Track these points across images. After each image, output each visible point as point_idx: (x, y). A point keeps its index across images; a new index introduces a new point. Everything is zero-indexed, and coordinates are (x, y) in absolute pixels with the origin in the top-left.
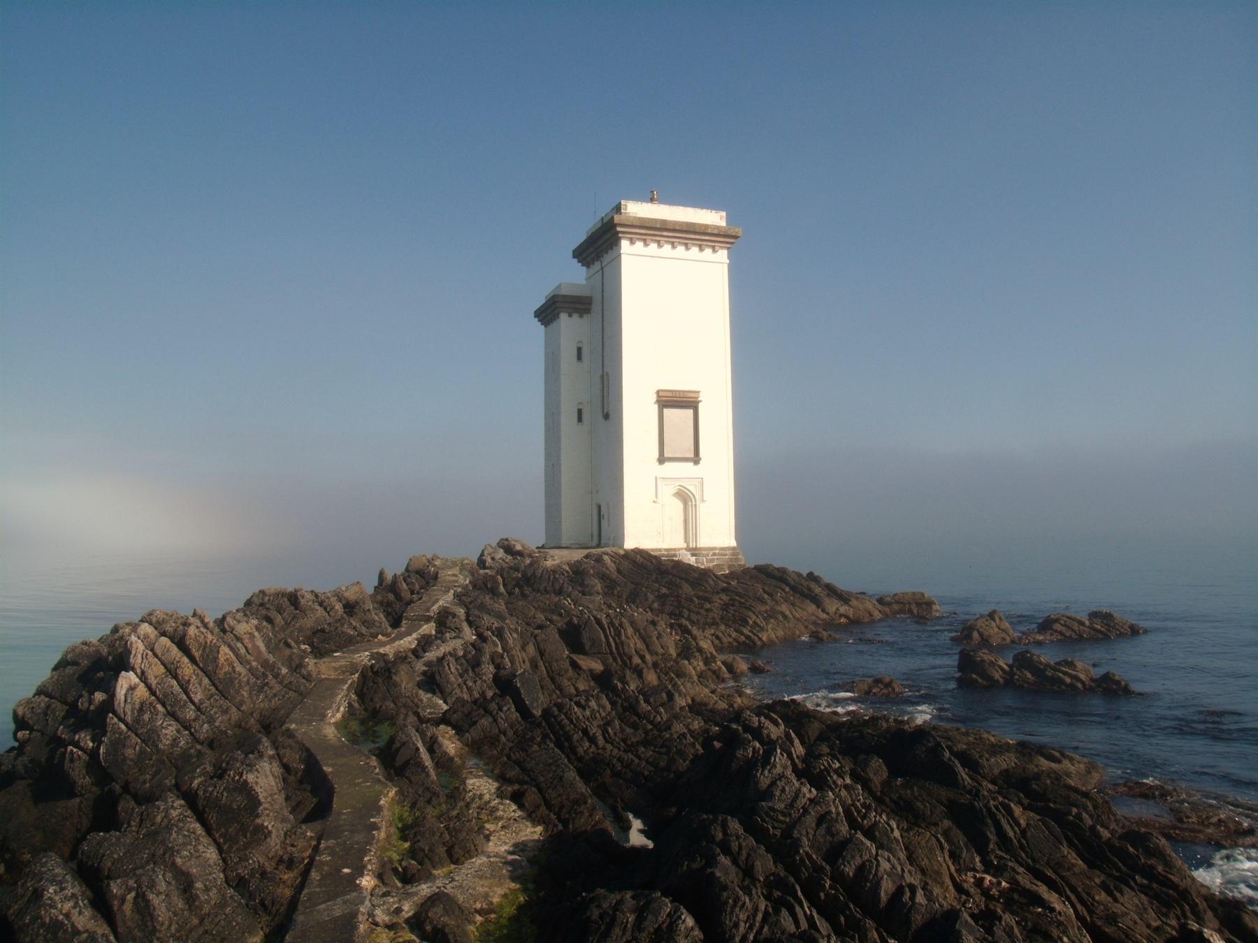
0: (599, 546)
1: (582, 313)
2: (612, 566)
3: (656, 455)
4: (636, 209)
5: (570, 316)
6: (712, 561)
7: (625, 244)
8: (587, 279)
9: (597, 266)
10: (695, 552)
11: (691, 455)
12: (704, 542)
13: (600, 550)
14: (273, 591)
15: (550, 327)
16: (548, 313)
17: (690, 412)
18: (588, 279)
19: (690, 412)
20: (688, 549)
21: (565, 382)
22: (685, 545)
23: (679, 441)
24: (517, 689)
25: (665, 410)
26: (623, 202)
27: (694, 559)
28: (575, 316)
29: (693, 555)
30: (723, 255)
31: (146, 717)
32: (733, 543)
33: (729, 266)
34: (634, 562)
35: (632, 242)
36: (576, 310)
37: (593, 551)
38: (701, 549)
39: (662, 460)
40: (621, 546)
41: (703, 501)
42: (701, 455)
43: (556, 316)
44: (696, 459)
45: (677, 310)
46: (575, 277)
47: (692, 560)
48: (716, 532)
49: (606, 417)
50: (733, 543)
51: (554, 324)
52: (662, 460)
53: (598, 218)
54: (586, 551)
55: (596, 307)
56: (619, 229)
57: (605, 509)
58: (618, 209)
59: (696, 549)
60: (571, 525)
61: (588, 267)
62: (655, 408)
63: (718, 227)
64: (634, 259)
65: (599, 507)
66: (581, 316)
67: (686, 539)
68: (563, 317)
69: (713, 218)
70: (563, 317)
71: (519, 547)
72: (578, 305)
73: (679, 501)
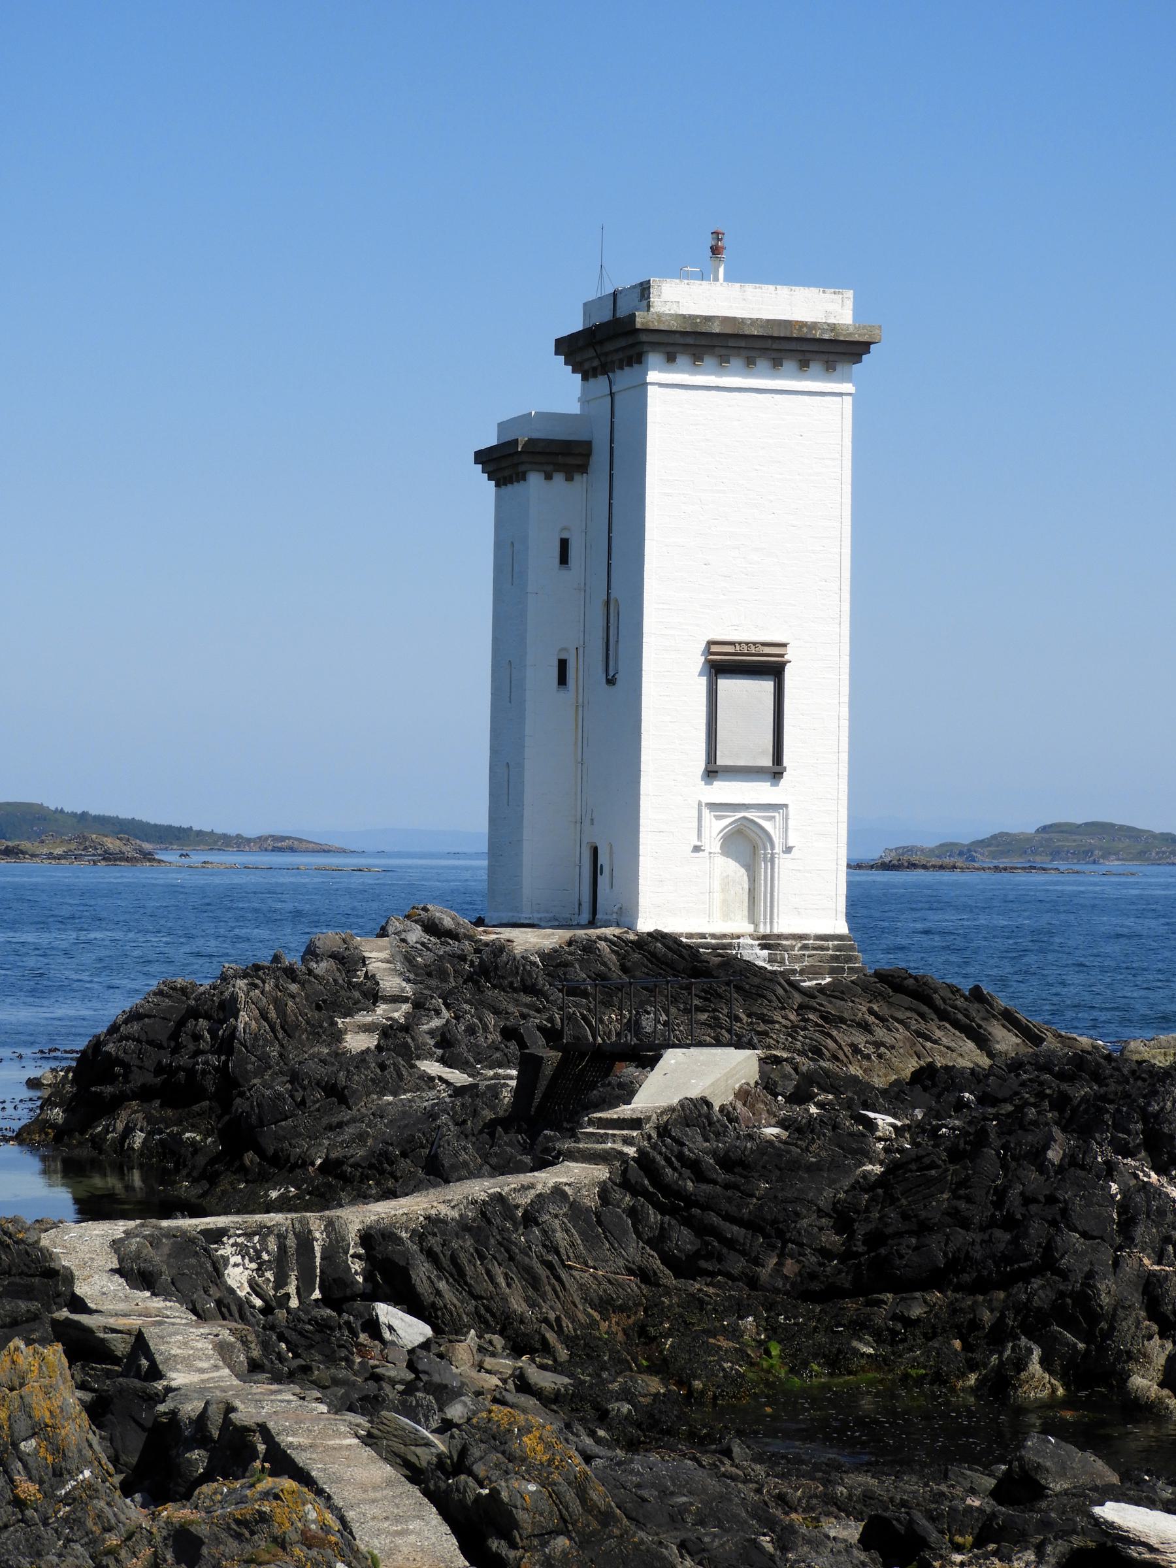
0: (592, 924)
3: (702, 765)
4: (680, 298)
5: (548, 477)
10: (769, 942)
11: (767, 761)
12: (785, 924)
13: (593, 932)
14: (34, 1155)
15: (509, 489)
16: (504, 462)
17: (768, 685)
18: (584, 400)
22: (750, 929)
23: (745, 741)
25: (724, 684)
28: (559, 478)
29: (764, 947)
32: (842, 928)
34: (653, 956)
36: (560, 468)
37: (581, 933)
38: (780, 936)
39: (712, 772)
40: (626, 913)
42: (787, 760)
44: (776, 772)
45: (743, 501)
46: (560, 393)
47: (759, 957)
49: (611, 681)
50: (842, 928)
52: (712, 772)
54: (567, 934)
56: (644, 338)
57: (601, 871)
58: (644, 290)
60: (544, 863)
61: (585, 378)
62: (701, 684)
64: (680, 411)
65: (595, 850)
66: (569, 478)
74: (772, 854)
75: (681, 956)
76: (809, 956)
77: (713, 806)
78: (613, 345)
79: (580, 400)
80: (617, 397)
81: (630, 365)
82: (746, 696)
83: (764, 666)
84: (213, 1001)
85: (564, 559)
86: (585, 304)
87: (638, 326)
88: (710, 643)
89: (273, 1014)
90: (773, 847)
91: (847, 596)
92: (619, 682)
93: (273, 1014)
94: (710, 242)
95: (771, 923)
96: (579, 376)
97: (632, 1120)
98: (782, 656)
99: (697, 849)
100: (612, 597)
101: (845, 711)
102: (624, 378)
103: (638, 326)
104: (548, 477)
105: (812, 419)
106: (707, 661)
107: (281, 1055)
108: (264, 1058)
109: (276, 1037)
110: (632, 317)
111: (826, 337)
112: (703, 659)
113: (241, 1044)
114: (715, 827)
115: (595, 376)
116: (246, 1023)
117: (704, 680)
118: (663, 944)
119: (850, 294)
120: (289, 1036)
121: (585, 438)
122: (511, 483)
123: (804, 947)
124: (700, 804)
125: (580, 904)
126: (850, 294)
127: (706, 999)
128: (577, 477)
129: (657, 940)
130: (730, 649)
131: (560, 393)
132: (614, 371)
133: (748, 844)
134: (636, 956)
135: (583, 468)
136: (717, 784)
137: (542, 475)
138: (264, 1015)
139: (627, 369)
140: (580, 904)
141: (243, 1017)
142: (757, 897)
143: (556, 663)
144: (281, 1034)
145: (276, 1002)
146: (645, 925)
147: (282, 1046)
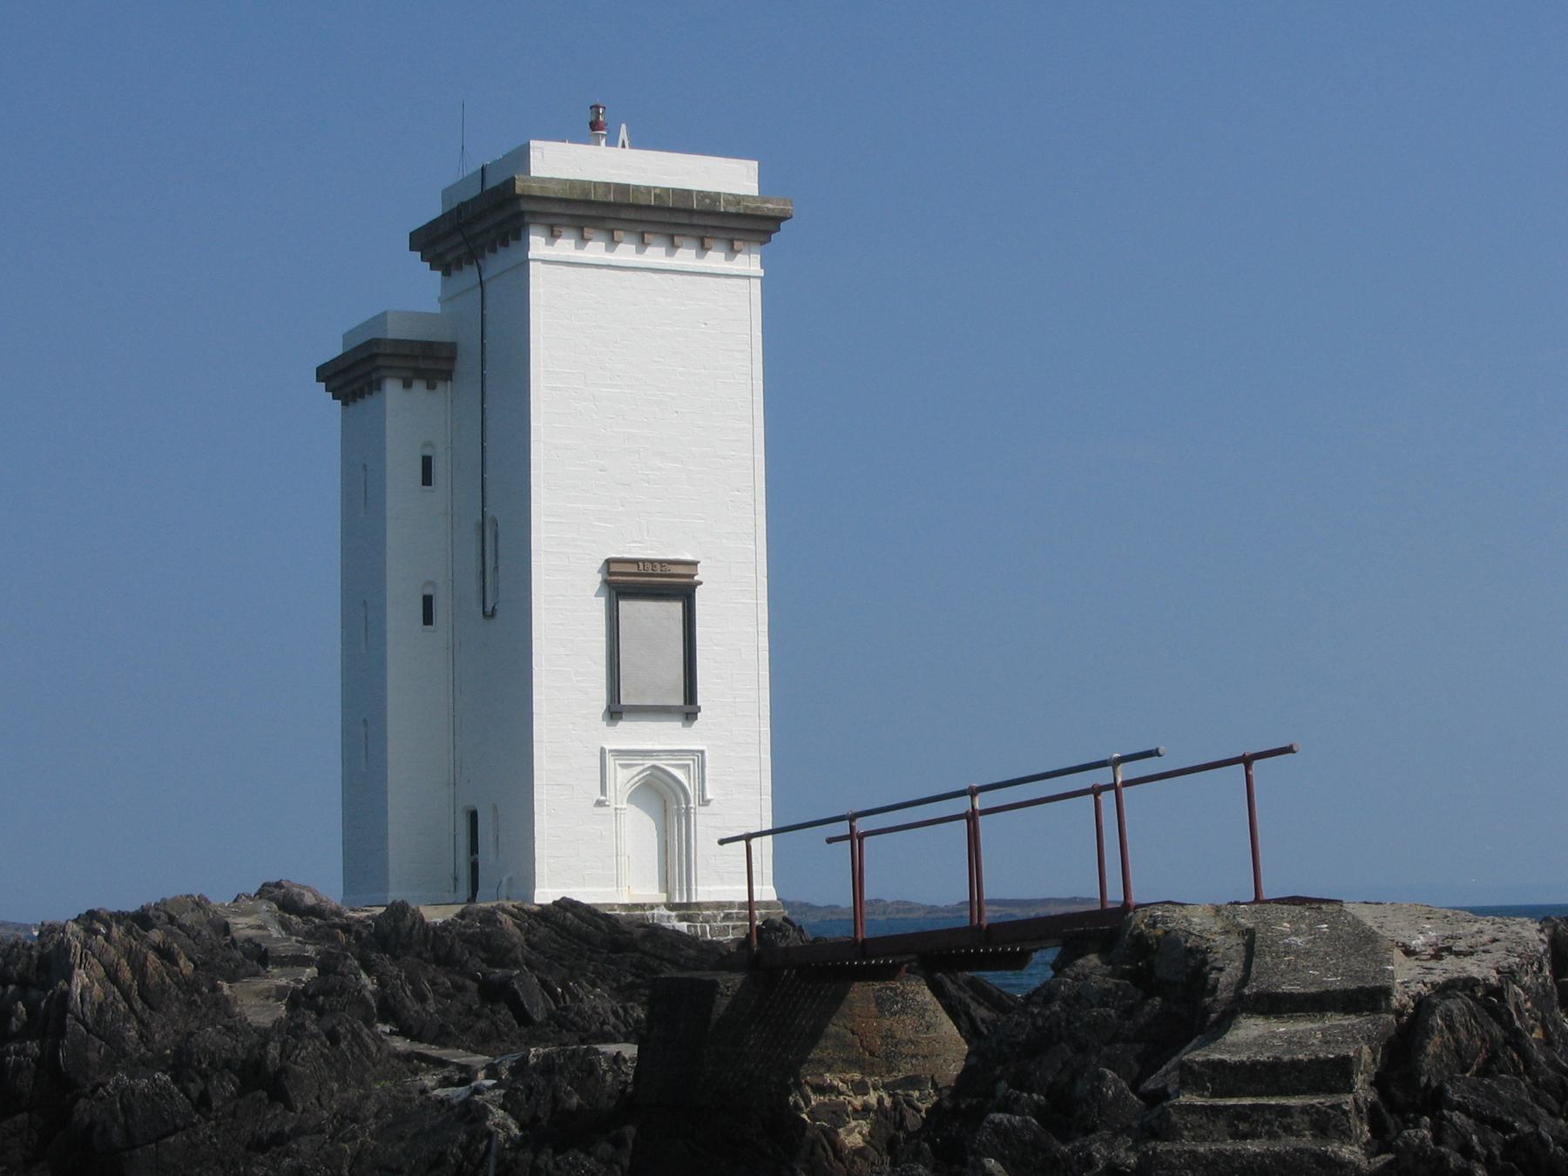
1: (435, 384)
2: (517, 936)
4: (556, 162)
5: (407, 385)
6: (725, 930)
7: (538, 245)
8: (442, 301)
9: (468, 276)
10: (687, 910)
11: (678, 700)
12: (705, 891)
16: (354, 375)
17: (676, 608)
18: (445, 300)
19: (676, 608)
20: (671, 906)
21: (395, 536)
22: (663, 898)
23: (653, 673)
24: (515, 993)
25: (624, 605)
26: (533, 143)
27: (685, 924)
28: (419, 387)
29: (682, 918)
30: (749, 263)
31: (109, 1017)
33: (766, 283)
35: (553, 235)
36: (420, 374)
38: (698, 905)
39: (615, 712)
41: (705, 802)
43: (374, 386)
44: (689, 710)
45: (645, 397)
46: (415, 296)
48: (729, 879)
49: (489, 615)
51: (369, 402)
52: (615, 712)
53: (474, 167)
55: (466, 364)
56: (524, 206)
57: (492, 817)
58: (522, 155)
59: (688, 906)
61: (447, 273)
63: (738, 199)
64: (572, 295)
65: (473, 817)
66: (431, 387)
67: (665, 884)
68: (392, 388)
69: (732, 178)
70: (392, 388)
71: (309, 900)
72: (427, 362)
73: (647, 809)
74: (688, 809)
75: (597, 927)
76: (734, 928)
77: (619, 753)
78: (485, 227)
79: (439, 300)
80: (489, 288)
81: (505, 244)
82: (652, 620)
83: (668, 585)
84: (30, 956)
85: (427, 479)
86: (444, 192)
87: (518, 191)
88: (608, 562)
89: (126, 974)
90: (688, 801)
91: (762, 508)
92: (499, 615)
93: (126, 974)
94: (589, 117)
95: (689, 890)
96: (439, 273)
97: (1318, 1064)
98: (692, 576)
99: (600, 803)
100: (489, 515)
101: (764, 642)
102: (496, 263)
103: (518, 191)
104: (407, 385)
105: (721, 297)
106: (606, 582)
107: (141, 1037)
108: (114, 1040)
109: (131, 1008)
110: (511, 183)
111: (732, 209)
112: (599, 578)
113: (77, 1019)
114: (623, 778)
115: (460, 268)
116: (84, 988)
117: (602, 602)
118: (575, 915)
119: (756, 164)
120: (151, 1008)
121: (448, 339)
122: (362, 397)
123: (727, 917)
124: (603, 751)
125: (456, 879)
126: (756, 164)
127: (638, 976)
128: (441, 386)
129: (566, 910)
130: (633, 569)
131: (415, 296)
132: (483, 256)
133: (664, 796)
134: (543, 930)
135: (447, 375)
136: (623, 725)
137: (400, 383)
138: (112, 976)
139: (501, 250)
140: (456, 879)
141: (80, 978)
142: (674, 856)
143: (420, 599)
144: (138, 1005)
145: (130, 954)
146: (545, 895)
147: (141, 1021)
